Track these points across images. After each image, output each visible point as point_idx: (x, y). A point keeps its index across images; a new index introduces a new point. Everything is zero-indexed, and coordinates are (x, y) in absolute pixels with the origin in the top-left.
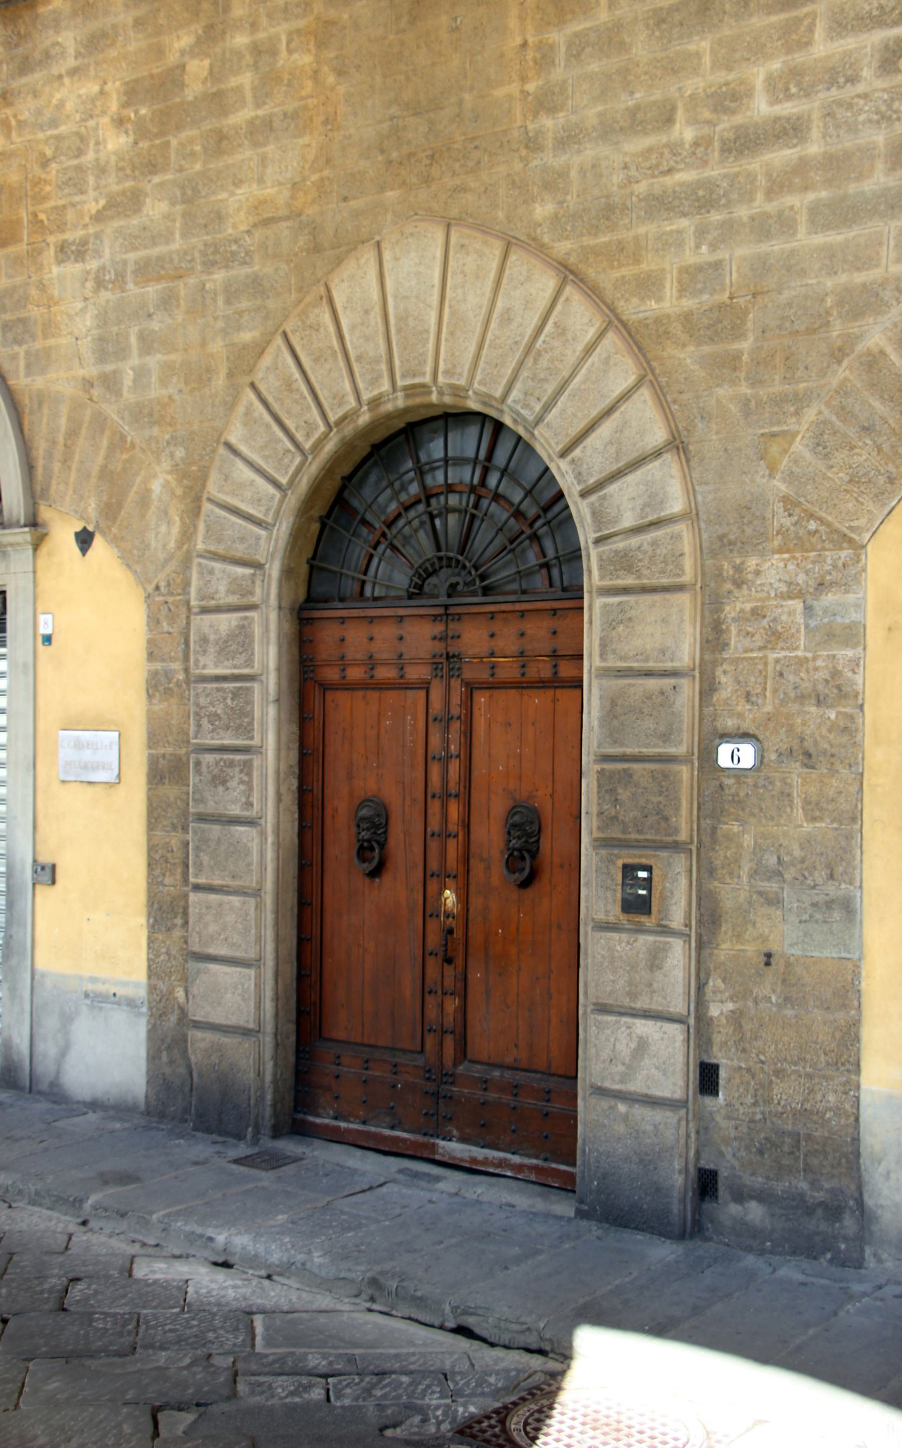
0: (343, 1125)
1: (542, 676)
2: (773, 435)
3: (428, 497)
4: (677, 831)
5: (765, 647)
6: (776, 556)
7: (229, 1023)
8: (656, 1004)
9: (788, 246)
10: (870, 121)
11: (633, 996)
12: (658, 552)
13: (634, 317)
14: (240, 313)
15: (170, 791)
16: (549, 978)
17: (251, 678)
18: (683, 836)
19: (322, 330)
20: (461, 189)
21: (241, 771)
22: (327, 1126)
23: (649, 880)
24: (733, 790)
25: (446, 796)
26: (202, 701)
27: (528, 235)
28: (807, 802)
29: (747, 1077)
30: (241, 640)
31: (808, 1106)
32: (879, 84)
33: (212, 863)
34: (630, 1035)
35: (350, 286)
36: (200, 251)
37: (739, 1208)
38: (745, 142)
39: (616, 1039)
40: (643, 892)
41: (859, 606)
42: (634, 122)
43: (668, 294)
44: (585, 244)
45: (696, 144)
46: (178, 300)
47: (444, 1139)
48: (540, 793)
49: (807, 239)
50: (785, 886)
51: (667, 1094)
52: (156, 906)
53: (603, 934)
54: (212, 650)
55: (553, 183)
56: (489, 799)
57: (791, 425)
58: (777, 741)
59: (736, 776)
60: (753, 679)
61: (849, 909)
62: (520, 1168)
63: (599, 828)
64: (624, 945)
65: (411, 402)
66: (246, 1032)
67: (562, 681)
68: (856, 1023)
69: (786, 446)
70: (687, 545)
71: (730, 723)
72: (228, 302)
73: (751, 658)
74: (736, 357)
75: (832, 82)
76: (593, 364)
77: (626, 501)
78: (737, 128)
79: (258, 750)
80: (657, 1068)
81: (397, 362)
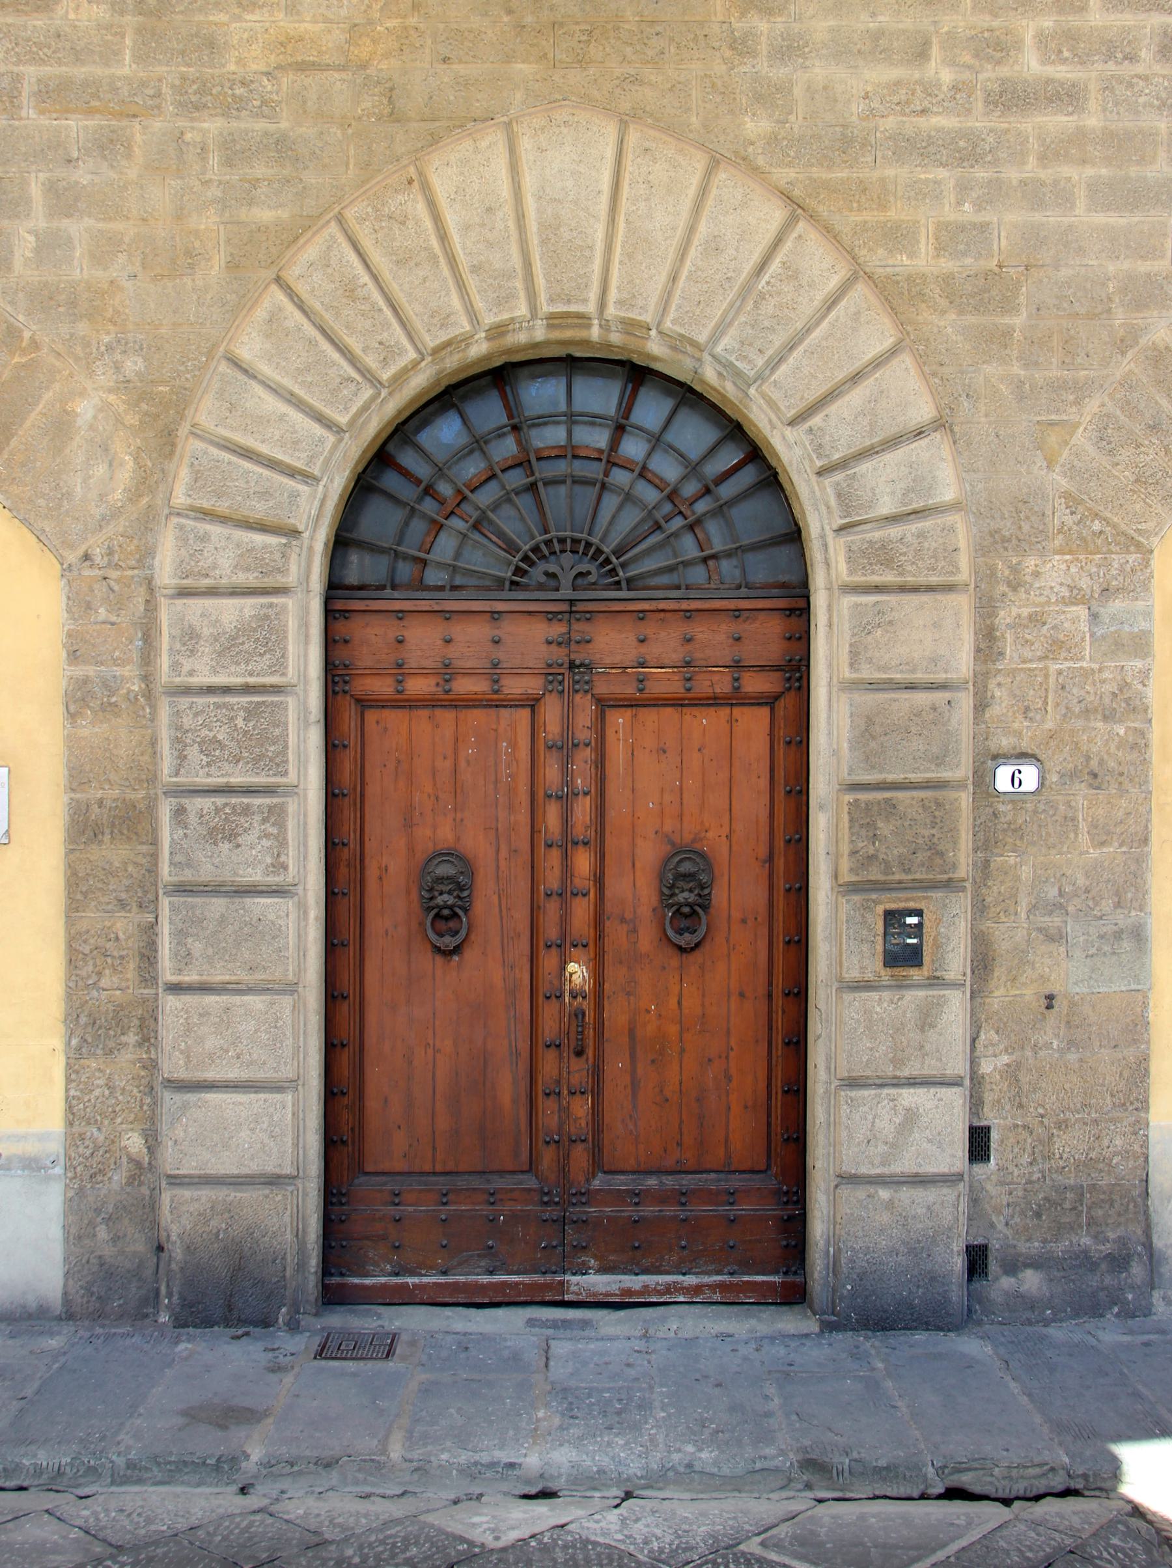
0: (411, 1280)
1: (718, 690)
2: (1052, 424)
3: (611, 464)
4: (954, 866)
5: (1047, 657)
6: (1057, 557)
7: (245, 1171)
8: (930, 1068)
9: (1066, 220)
10: (1152, 106)
11: (897, 1062)
12: (926, 545)
13: (880, 270)
14: (255, 183)
15: (114, 853)
16: (727, 1058)
17: (277, 689)
18: (961, 872)
19: (410, 224)
20: (636, 80)
21: (264, 821)
22: (384, 1286)
23: (919, 926)
24: (1009, 817)
25: (568, 844)
26: (187, 721)
27: (736, 153)
28: (1094, 826)
29: (1025, 1134)
30: (266, 636)
31: (1093, 1155)
32: (1157, 68)
33: (210, 951)
34: (894, 1108)
35: (462, 173)
36: (173, 86)
37: (1013, 1280)
38: (1011, 98)
39: (875, 1117)
40: (914, 941)
41: (1148, 614)
42: (877, 46)
43: (923, 250)
44: (815, 176)
45: (955, 88)
46: (129, 148)
47: (574, 1274)
48: (710, 835)
49: (1084, 216)
50: (1069, 920)
51: (943, 1169)
52: (83, 1020)
53: (857, 995)
54: (205, 649)
55: (768, 96)
56: (634, 845)
57: (1071, 414)
58: (1060, 760)
59: (1012, 801)
60: (1032, 692)
61: (1139, 936)
62: (698, 1289)
63: (851, 870)
64: (885, 1005)
65: (557, 335)
66: (273, 1181)
67: (747, 696)
68: (1146, 1059)
69: (1068, 437)
70: (962, 540)
71: (1005, 743)
72: (228, 163)
73: (1029, 669)
74: (1008, 333)
75: (1109, 56)
76: (838, 317)
77: (883, 483)
78: (1003, 81)
79: (291, 790)
80: (930, 1141)
81: (541, 282)
